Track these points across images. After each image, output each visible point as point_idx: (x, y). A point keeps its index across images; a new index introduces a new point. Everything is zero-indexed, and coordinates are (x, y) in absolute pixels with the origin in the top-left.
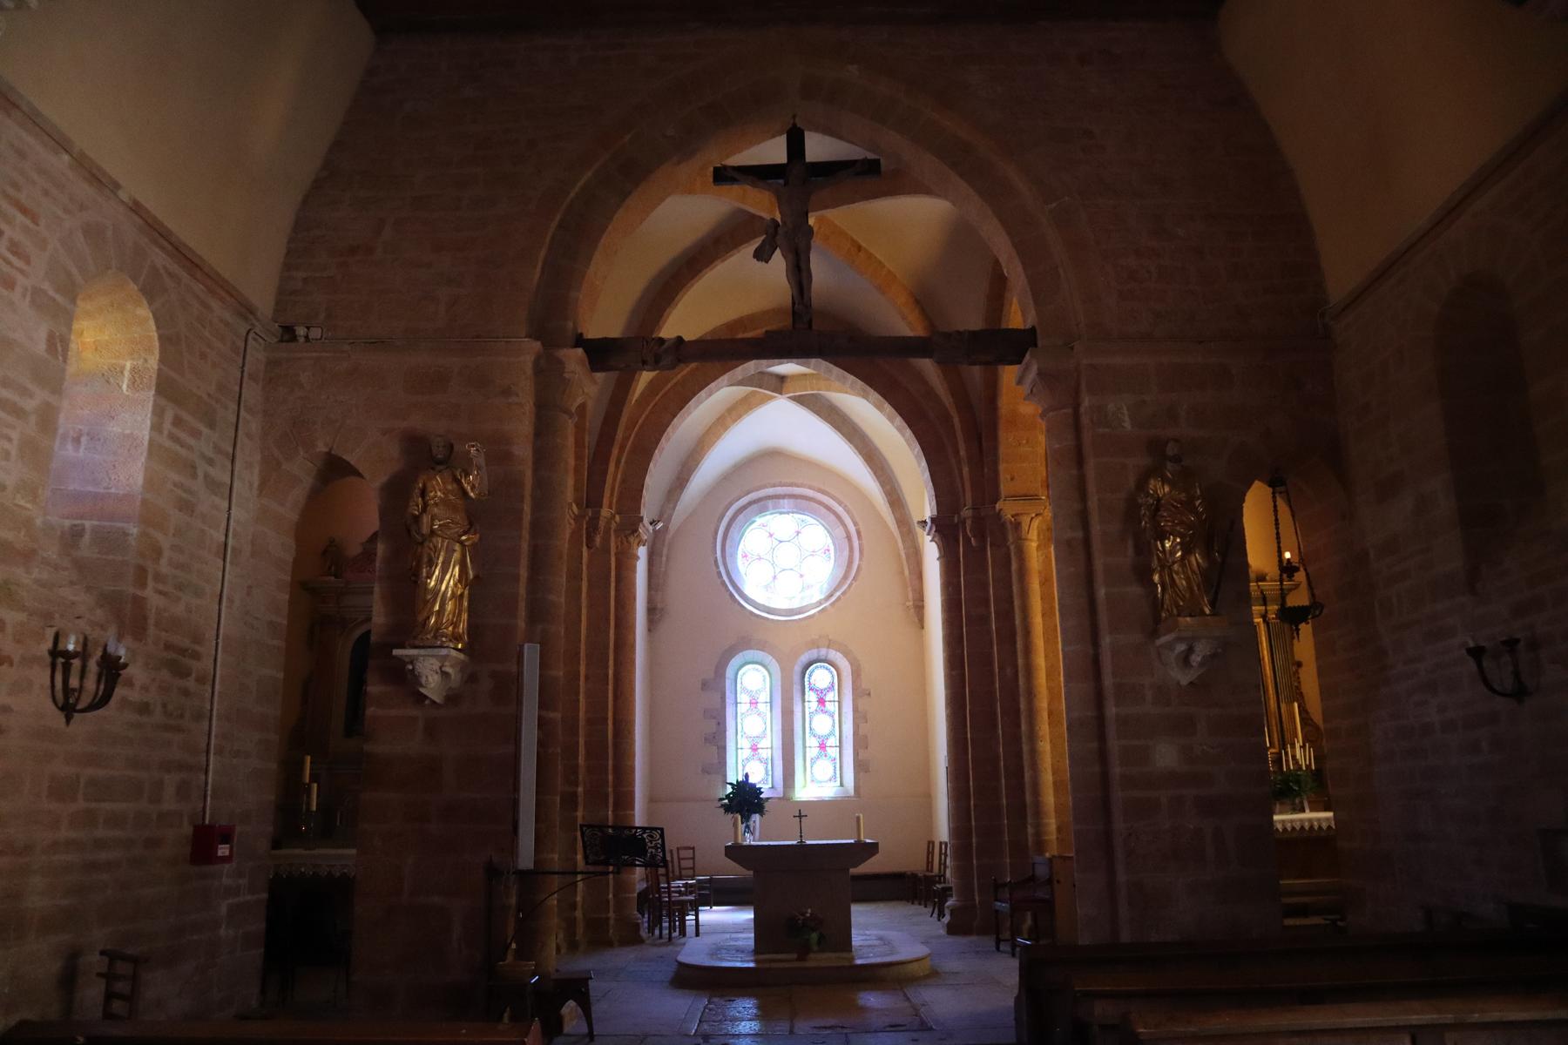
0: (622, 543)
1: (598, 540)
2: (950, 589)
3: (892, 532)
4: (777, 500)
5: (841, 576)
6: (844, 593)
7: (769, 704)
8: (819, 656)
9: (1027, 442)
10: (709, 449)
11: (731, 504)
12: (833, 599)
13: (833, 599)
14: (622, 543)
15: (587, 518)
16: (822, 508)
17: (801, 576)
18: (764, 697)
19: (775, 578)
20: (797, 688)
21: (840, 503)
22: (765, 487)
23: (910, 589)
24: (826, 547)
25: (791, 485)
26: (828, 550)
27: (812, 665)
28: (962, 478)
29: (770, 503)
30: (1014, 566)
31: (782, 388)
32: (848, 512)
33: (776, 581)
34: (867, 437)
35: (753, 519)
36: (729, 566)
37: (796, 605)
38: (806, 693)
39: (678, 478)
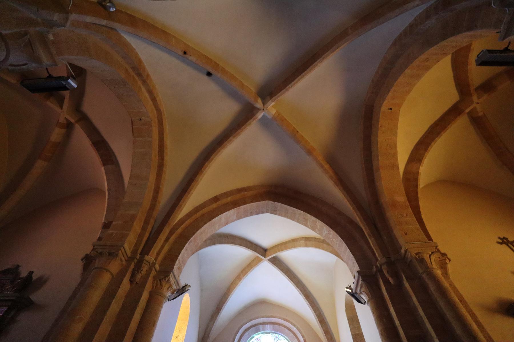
0: (157, 285)
1: (139, 276)
2: (384, 320)
4: (264, 325)
9: (406, 215)
10: (232, 291)
11: (242, 326)
14: (157, 285)
15: (136, 261)
16: (286, 329)
21: (295, 326)
22: (257, 318)
25: (271, 317)
28: (370, 248)
29: (261, 327)
30: (432, 288)
32: (299, 330)
34: (305, 286)
35: (253, 336)
39: (217, 308)
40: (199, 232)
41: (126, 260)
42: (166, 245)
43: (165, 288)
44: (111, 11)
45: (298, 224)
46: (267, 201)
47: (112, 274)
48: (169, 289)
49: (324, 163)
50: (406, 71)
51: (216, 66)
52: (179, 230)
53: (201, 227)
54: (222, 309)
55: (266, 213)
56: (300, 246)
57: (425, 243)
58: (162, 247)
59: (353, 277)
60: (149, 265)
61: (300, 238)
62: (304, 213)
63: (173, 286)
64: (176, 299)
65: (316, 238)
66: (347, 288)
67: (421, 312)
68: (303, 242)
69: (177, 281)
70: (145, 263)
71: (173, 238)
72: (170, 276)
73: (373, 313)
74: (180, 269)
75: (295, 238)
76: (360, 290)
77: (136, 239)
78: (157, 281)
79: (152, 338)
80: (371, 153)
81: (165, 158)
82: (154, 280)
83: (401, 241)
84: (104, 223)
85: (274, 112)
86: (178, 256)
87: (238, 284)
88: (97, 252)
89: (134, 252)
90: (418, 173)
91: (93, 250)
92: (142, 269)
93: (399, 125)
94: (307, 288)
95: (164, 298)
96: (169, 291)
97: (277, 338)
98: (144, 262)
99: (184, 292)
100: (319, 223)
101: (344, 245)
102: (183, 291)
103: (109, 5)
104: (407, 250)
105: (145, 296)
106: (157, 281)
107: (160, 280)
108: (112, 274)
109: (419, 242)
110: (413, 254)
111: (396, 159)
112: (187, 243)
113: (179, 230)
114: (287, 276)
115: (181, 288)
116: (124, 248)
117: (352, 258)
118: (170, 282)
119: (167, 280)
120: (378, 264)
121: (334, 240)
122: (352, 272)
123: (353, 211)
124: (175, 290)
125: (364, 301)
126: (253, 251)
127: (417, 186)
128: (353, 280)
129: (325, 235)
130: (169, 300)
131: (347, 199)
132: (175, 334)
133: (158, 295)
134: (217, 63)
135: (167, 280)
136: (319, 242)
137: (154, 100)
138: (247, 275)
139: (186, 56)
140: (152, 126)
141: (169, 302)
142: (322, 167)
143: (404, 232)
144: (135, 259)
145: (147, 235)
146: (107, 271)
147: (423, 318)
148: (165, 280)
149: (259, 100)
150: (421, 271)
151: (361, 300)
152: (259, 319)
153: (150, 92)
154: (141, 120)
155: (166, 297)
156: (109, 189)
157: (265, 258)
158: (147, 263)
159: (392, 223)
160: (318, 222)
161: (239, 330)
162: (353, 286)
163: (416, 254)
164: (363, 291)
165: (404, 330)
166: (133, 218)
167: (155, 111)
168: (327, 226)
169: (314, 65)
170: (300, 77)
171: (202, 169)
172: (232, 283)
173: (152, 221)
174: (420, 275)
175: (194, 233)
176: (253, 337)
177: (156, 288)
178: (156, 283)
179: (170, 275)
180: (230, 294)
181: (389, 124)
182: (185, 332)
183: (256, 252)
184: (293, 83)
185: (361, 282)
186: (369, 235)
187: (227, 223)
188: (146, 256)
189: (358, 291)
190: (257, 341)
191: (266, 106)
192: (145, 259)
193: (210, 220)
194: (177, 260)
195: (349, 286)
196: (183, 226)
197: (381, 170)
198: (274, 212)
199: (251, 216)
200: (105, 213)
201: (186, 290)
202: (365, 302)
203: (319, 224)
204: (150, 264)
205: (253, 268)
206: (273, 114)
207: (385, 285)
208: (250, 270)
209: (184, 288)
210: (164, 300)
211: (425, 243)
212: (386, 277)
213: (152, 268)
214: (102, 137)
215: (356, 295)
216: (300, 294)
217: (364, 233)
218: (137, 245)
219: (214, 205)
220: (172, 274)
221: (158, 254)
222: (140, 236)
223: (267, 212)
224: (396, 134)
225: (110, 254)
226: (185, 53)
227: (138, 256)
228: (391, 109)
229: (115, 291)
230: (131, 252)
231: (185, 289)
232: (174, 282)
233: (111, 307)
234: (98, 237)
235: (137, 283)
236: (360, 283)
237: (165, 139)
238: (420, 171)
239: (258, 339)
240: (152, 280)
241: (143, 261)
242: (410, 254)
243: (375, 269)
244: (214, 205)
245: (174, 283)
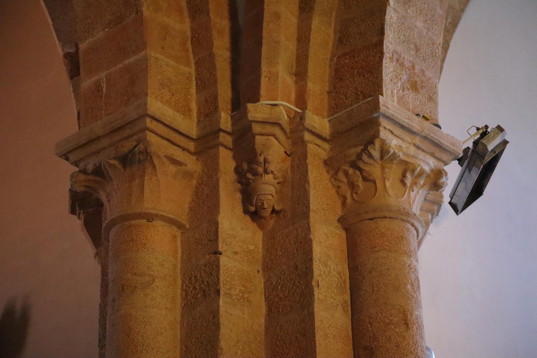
0: (352, 185)
14: (352, 185)
15: (227, 140)
41: (194, 154)
43: (388, 184)
47: (171, 222)
48: (409, 181)
70: (262, 134)
72: (383, 134)
77: (193, 61)
78: (346, 173)
82: (334, 177)
86: (380, 43)
98: (256, 128)
106: (346, 173)
108: (171, 222)
116: (153, 118)
119: (376, 154)
130: (460, 208)
135: (376, 154)
144: (222, 134)
146: (150, 217)
148: (370, 156)
158: (269, 129)
177: (354, 196)
178: (345, 180)
179: (381, 128)
188: (250, 106)
192: (250, 119)
194: (386, 62)
210: (409, 226)
220: (384, 122)
231: (485, 147)
232: (418, 148)
233: (223, 320)
240: (326, 177)
241: (250, 128)
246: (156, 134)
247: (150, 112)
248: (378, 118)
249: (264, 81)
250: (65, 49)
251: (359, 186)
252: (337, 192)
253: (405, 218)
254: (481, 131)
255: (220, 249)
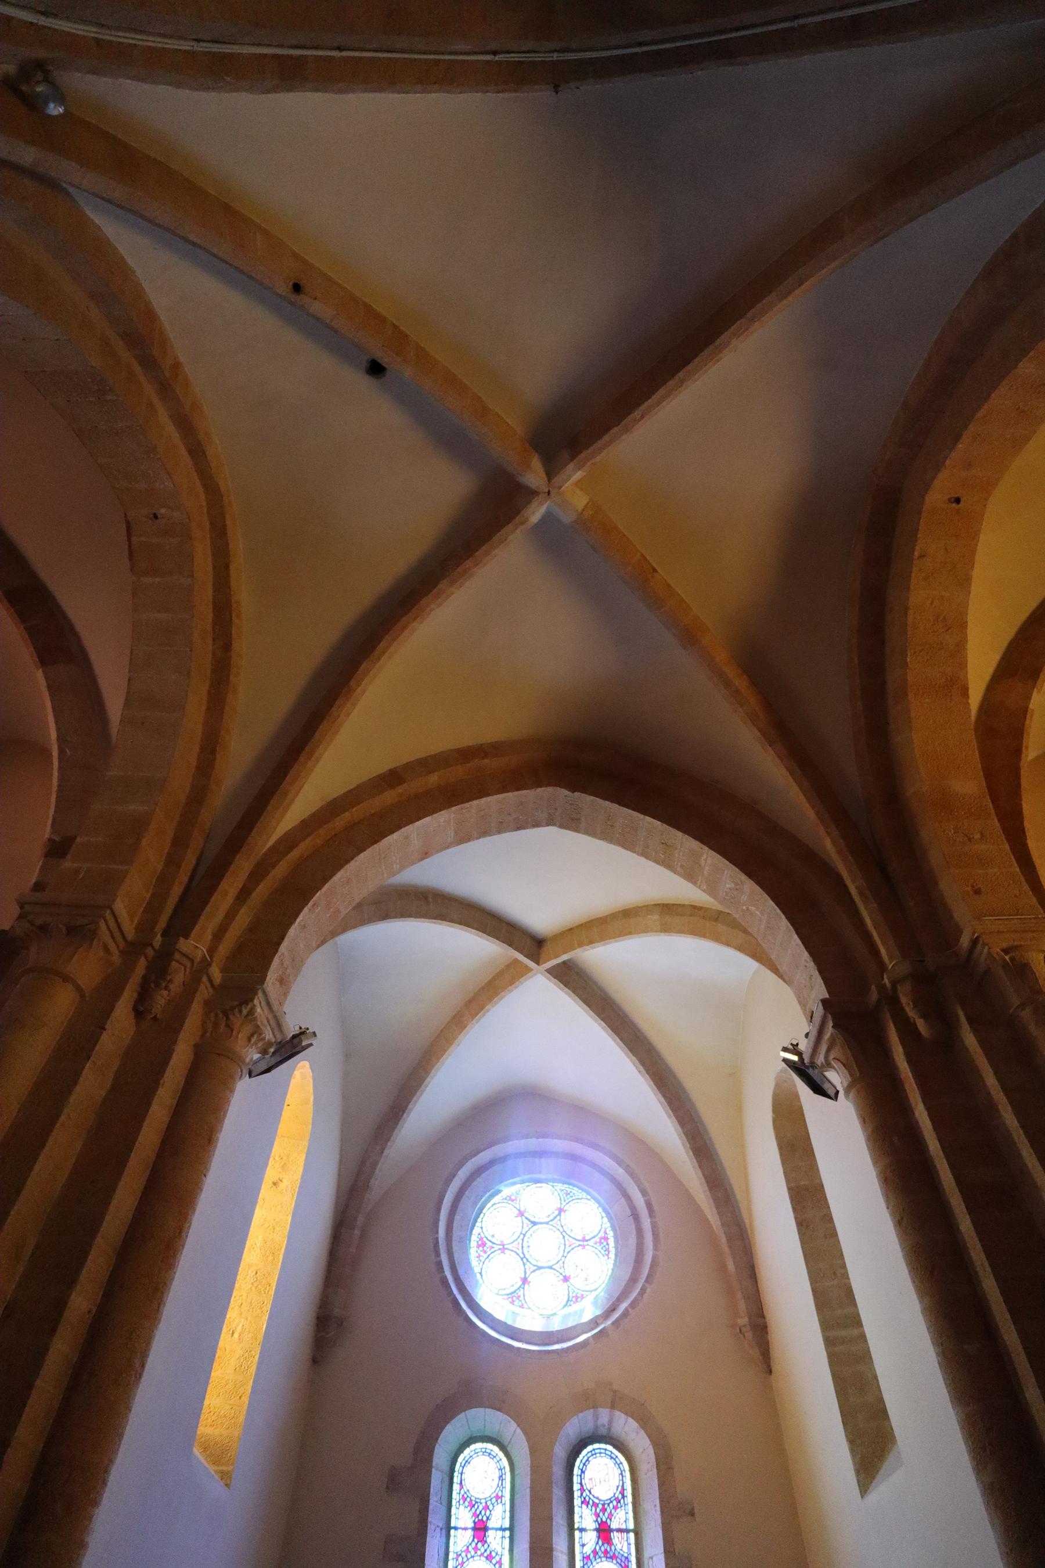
0: (216, 1025)
1: (161, 1000)
2: (895, 1140)
3: (707, 1220)
5: (627, 1277)
6: (633, 1305)
7: (507, 1533)
8: (596, 1427)
9: (982, 835)
10: (438, 1059)
12: (616, 1315)
13: (616, 1315)
15: (150, 952)
17: (566, 1279)
18: (499, 1517)
19: (525, 1281)
20: (558, 1494)
23: (739, 1295)
24: (602, 1234)
26: (606, 1239)
27: (585, 1447)
31: (539, 954)
33: (526, 1286)
35: (497, 1188)
36: (456, 1255)
37: (556, 1325)
38: (577, 1510)
40: (339, 875)
41: (119, 951)
42: (243, 911)
44: (50, 115)
45: (643, 860)
46: (550, 789)
48: (253, 1040)
49: (731, 672)
50: (1021, 365)
51: (399, 340)
52: (281, 870)
53: (347, 861)
54: (407, 1111)
55: (548, 825)
56: (646, 930)
57: (1033, 920)
58: (230, 916)
59: (807, 1019)
60: (192, 965)
61: (646, 906)
62: (665, 825)
63: (267, 1032)
64: (273, 1072)
65: (694, 907)
66: (785, 1049)
67: (1009, 1118)
68: (656, 917)
69: (276, 1017)
70: (178, 962)
71: (262, 890)
72: (256, 1002)
73: (864, 1121)
74: (283, 982)
75: (629, 907)
76: (826, 1057)
78: (217, 1015)
79: (205, 1176)
80: (883, 643)
81: (236, 645)
83: (961, 911)
84: (50, 840)
85: (580, 501)
86: (279, 944)
87: (455, 1038)
88: (31, 923)
89: (145, 927)
90: (1024, 712)
91: (21, 917)
92: (169, 978)
93: (981, 557)
94: (663, 1060)
95: (239, 1066)
96: (253, 1045)
97: (568, 1196)
98: (177, 956)
99: (297, 1050)
100: (709, 858)
101: (784, 923)
102: (294, 1047)
103: (42, 91)
104: (977, 939)
105: (182, 1055)
106: (217, 1015)
107: (226, 1013)
109: (1017, 915)
110: (996, 950)
111: (963, 665)
112: (303, 908)
113: (281, 870)
114: (602, 1020)
115: (288, 1039)
117: (806, 964)
118: (255, 1019)
119: (245, 1012)
120: (886, 980)
121: (753, 908)
122: (803, 1004)
123: (818, 821)
124: (270, 1044)
125: (835, 1091)
126: (503, 942)
127: (1017, 752)
128: (805, 1027)
129: (727, 895)
130: (253, 1075)
131: (800, 786)
132: (271, 1173)
133: (219, 1055)
134: (401, 332)
135: (245, 1012)
136: (704, 918)
137: (197, 452)
138: (484, 1015)
139: (303, 299)
140: (191, 539)
141: (251, 1079)
142: (727, 683)
143: (973, 887)
144: (150, 948)
145: (183, 877)
146: (66, 979)
147: (1014, 1134)
148: (240, 1012)
149: (536, 463)
150: (1015, 1001)
151: (826, 1086)
152: (517, 1141)
153: (185, 423)
154: (155, 517)
155: (243, 1062)
156: (61, 739)
157: (538, 965)
158: (184, 960)
159: (935, 857)
160: (705, 856)
161: (458, 1171)
162: (804, 1046)
163: (1006, 951)
164: (834, 1058)
165: (952, 1167)
166: (138, 826)
167: (200, 489)
168: (734, 867)
169: (718, 342)
170: (671, 383)
171: (352, 683)
172: (438, 1037)
173: (197, 841)
174: (1012, 1011)
175: (325, 880)
176: (499, 1192)
177: (214, 1034)
178: (213, 1019)
179: (256, 997)
180: (431, 1069)
181: (946, 549)
182: (301, 1169)
183: (510, 945)
184: (646, 404)
185: (829, 1030)
186: (861, 894)
187: (426, 855)
188: (182, 940)
189: (820, 1059)
190: (509, 1202)
191: (556, 481)
192: (177, 948)
193: (375, 842)
195: (792, 1044)
196: (295, 854)
197: (911, 697)
198: (572, 822)
199: (499, 832)
200: (51, 812)
201: (304, 1044)
202: (837, 1092)
203: (709, 862)
204: (195, 964)
205: (500, 996)
206: (580, 510)
207: (903, 1043)
208: (490, 999)
209: (296, 1041)
211: (1036, 918)
212: (907, 1018)
213: (201, 978)
214: (35, 577)
215: (810, 1071)
216: (638, 1073)
217: (846, 887)
218: (153, 908)
219: (389, 797)
220: (260, 994)
221: (218, 936)
222: (164, 881)
223: (550, 822)
224: (965, 582)
225: (73, 930)
226: (297, 288)
227: (158, 941)
228: (958, 501)
229: (93, 1040)
230: (136, 929)
232: (268, 1021)
234: (34, 881)
235: (155, 1018)
236: (827, 1036)
237: (233, 584)
238: (1031, 706)
239: (513, 1197)
241: (173, 953)
242: (986, 950)
243: (874, 996)
244: (389, 797)
245: (265, 1022)
246: (107, 924)
247: (113, 906)
248: (258, 989)
249: (197, 927)
250: (52, 835)
251: (220, 1028)
252: (202, 1025)
253: (241, 1064)
254: (301, 1031)
255: (106, 1027)
